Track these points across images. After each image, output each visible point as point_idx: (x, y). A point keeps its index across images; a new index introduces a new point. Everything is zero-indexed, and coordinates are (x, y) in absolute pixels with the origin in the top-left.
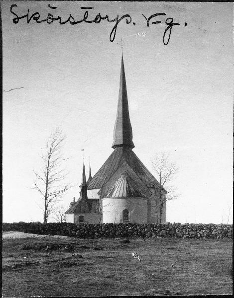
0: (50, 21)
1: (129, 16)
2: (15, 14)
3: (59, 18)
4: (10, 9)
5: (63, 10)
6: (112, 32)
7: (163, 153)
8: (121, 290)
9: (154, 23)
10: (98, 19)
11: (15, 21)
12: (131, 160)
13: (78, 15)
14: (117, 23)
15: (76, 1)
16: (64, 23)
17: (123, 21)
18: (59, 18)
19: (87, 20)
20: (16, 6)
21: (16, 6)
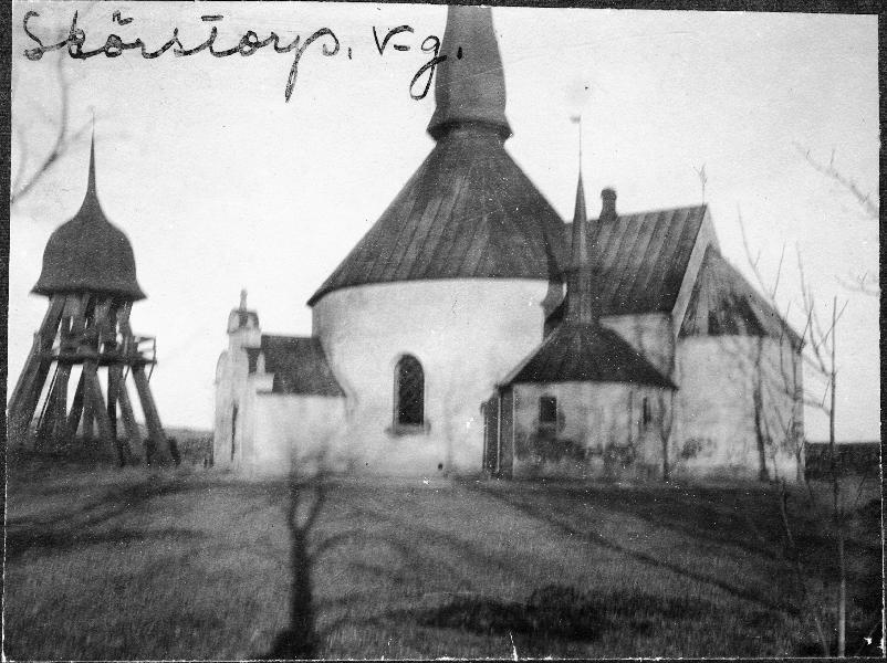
0: (247, 48)
1: (330, 32)
2: (37, 40)
3: (139, 43)
4: (117, 34)
5: (151, 23)
6: (418, 75)
7: (412, 630)
8: (443, 654)
9: (399, 48)
10: (250, 43)
11: (38, 54)
12: (747, 314)
13: (195, 34)
14: (298, 57)
15: (197, 2)
16: (155, 55)
17: (313, 53)
18: (139, 43)
19: (37, 45)
20: (410, 30)
21: (410, 30)
